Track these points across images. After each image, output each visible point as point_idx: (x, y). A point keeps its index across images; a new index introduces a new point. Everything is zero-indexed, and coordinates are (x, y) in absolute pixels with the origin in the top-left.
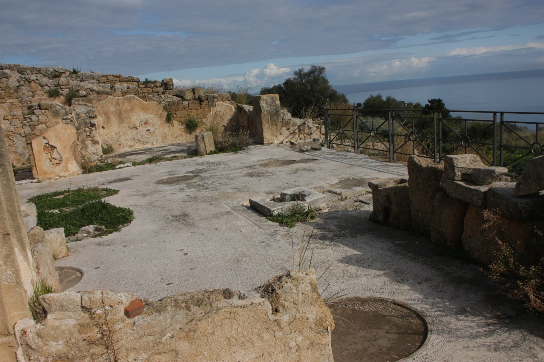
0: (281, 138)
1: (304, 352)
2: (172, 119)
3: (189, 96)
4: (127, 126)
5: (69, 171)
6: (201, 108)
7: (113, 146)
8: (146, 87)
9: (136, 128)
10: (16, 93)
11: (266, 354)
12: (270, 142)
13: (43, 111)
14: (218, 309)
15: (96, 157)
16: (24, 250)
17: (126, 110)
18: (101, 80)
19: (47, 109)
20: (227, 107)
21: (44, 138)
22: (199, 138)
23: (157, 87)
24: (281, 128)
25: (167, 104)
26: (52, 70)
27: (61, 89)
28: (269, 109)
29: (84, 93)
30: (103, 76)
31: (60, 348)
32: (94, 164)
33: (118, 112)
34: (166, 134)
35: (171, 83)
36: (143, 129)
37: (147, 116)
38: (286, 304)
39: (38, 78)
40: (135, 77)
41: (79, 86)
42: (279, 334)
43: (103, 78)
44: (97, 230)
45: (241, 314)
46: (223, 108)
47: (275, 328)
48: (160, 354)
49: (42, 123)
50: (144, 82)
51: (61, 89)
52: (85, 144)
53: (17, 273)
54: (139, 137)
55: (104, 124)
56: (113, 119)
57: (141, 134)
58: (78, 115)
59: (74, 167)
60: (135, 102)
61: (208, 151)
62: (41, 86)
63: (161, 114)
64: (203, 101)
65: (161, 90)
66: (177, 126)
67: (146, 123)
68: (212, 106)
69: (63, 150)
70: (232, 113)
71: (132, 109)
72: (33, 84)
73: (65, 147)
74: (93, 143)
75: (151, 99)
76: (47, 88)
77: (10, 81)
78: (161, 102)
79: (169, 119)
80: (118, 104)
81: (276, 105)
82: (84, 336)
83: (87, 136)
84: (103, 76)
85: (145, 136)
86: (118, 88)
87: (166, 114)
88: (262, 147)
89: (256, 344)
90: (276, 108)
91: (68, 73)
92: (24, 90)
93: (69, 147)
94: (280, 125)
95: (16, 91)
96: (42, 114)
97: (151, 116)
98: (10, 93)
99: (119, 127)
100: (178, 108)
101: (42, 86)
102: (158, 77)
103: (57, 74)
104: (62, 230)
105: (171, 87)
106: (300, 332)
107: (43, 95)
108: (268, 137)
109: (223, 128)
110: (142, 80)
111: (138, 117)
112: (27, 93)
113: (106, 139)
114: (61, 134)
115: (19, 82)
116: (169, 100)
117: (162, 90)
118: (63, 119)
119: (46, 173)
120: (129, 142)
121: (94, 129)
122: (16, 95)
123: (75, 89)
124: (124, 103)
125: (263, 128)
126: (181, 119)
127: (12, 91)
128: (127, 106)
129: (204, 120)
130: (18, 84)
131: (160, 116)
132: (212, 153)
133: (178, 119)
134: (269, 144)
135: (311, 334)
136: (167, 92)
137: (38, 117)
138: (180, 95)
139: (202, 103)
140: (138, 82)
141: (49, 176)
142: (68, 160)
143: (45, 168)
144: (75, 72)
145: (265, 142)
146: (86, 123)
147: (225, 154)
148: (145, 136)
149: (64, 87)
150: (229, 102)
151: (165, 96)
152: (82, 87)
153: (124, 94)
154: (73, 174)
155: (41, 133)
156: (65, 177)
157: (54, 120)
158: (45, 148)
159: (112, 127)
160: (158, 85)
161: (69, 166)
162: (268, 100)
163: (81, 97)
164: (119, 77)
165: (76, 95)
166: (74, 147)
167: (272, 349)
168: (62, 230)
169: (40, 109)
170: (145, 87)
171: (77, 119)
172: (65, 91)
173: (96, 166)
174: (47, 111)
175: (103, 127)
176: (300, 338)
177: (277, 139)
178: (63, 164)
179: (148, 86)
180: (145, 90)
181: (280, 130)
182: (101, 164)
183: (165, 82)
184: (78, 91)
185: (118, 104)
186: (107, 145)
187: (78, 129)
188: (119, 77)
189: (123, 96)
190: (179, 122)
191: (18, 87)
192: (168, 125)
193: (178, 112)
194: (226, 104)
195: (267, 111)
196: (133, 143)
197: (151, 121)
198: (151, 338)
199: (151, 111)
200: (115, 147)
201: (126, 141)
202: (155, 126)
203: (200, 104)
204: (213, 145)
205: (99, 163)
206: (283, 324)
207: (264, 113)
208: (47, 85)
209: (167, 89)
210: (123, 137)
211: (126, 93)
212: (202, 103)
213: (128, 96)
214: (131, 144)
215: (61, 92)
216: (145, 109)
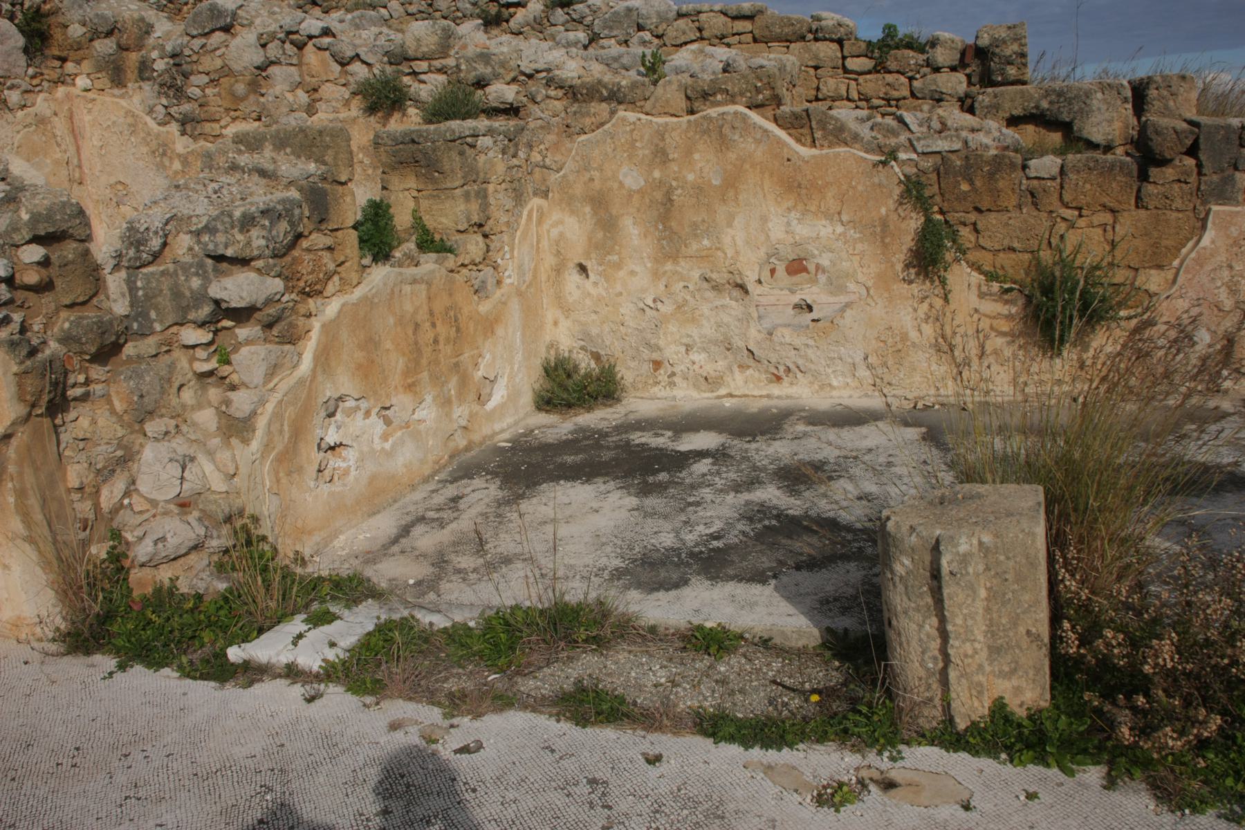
3: (1108, 122)
4: (696, 274)
6: (1139, 202)
8: (880, 68)
9: (742, 288)
10: (252, 98)
17: (700, 190)
23: (937, 70)
25: (927, 164)
27: (414, 74)
30: (680, 15)
33: (659, 195)
34: (904, 337)
36: (777, 296)
37: (803, 231)
43: (681, 23)
51: (414, 74)
54: (754, 335)
55: (587, 255)
56: (632, 230)
57: (767, 324)
60: (747, 145)
61: (970, 708)
62: (343, 65)
63: (884, 223)
64: (1163, 162)
65: (957, 83)
66: (974, 300)
67: (797, 267)
71: (731, 183)
75: (839, 135)
77: (236, 42)
78: (892, 155)
79: (927, 259)
80: (661, 155)
84: (680, 15)
85: (786, 335)
86: (678, 71)
87: (915, 222)
95: (255, 87)
97: (826, 229)
98: (233, 94)
99: (656, 275)
100: (996, 193)
105: (1012, 71)
107: (347, 103)
111: (758, 227)
112: (290, 97)
113: (594, 331)
115: (264, 46)
116: (942, 145)
124: (689, 152)
126: (1005, 259)
128: (705, 165)
129: (1153, 280)
130: (258, 57)
131: (882, 233)
133: (986, 259)
136: (985, 97)
139: (1153, 172)
140: (840, 42)
149: (423, 66)
152: (503, 64)
153: (699, 97)
159: (621, 274)
160: (942, 56)
164: (750, 18)
170: (874, 70)
175: (583, 269)
179: (892, 65)
180: (872, 85)
183: (984, 41)
185: (661, 155)
186: (597, 357)
188: (750, 18)
189: (692, 112)
190: (991, 277)
193: (992, 217)
196: (721, 365)
197: (825, 261)
199: (832, 203)
200: (626, 373)
203: (1143, 177)
209: (987, 80)
210: (672, 328)
211: (705, 96)
212: (1153, 172)
213: (713, 112)
214: (709, 369)
215: (414, 87)
216: (797, 188)
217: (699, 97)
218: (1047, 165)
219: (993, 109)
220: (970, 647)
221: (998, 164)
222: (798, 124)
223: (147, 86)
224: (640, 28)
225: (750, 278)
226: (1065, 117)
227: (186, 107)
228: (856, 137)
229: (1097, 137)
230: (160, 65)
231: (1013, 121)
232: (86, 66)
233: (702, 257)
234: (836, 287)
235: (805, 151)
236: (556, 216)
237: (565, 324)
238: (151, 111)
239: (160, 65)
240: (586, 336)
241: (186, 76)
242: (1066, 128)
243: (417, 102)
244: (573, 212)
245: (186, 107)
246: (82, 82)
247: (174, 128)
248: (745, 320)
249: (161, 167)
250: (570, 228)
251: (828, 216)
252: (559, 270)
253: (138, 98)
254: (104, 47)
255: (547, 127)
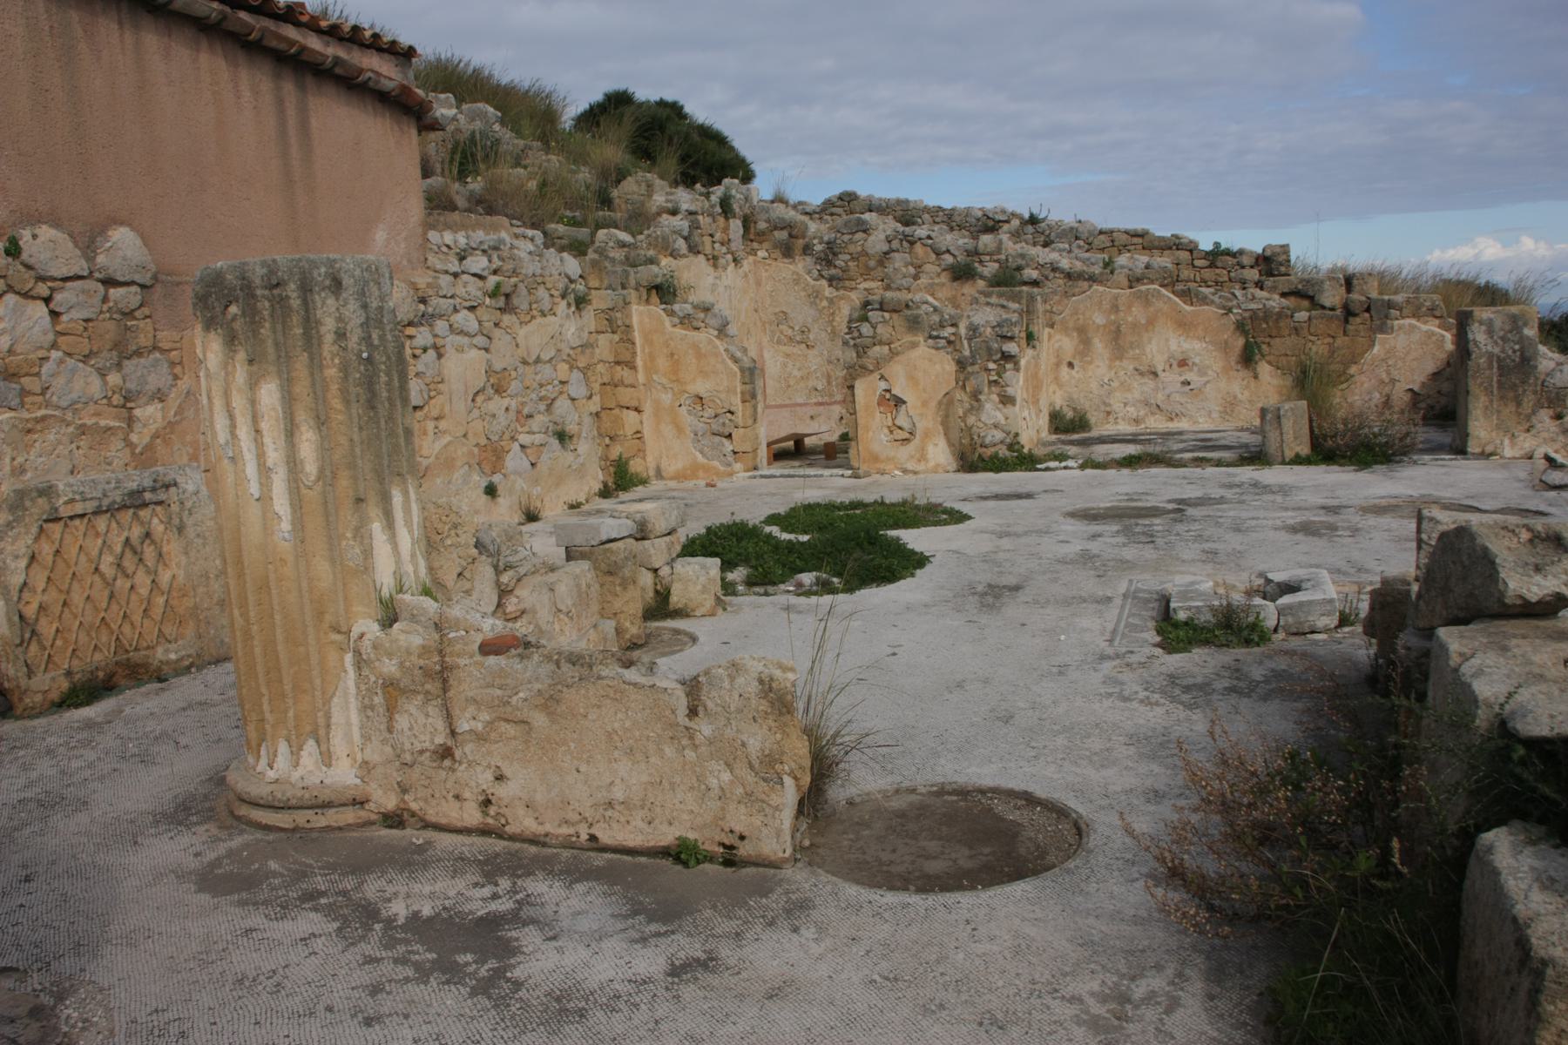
0: (1527, 443)
1: (732, 806)
2: (1257, 357)
3: (1332, 296)
5: (926, 460)
7: (1089, 416)
8: (1212, 265)
9: (1155, 374)
11: (666, 784)
12: (1489, 449)
13: (887, 315)
14: (599, 678)
15: (999, 435)
16: (390, 525)
17: (1135, 326)
18: (1096, 242)
19: (895, 311)
20: (1430, 334)
21: (882, 377)
22: (1269, 416)
23: (1243, 267)
24: (1534, 413)
25: (1247, 315)
26: (980, 214)
27: (981, 262)
28: (1496, 350)
29: (1034, 274)
31: (393, 669)
32: (989, 452)
35: (1282, 258)
36: (1172, 378)
37: (1186, 346)
38: (710, 704)
39: (933, 235)
40: (1189, 234)
41: (1023, 256)
42: (690, 755)
43: (1102, 237)
44: (818, 581)
45: (633, 697)
46: (1416, 337)
47: (685, 742)
48: (507, 721)
49: (881, 343)
50: (1207, 253)
51: (981, 262)
52: (978, 400)
53: (368, 553)
54: (1160, 397)
56: (1098, 345)
57: (1167, 391)
58: (974, 330)
59: (940, 453)
60: (1160, 304)
61: (1289, 454)
64: (1355, 315)
65: (1253, 275)
67: (1183, 363)
68: (1382, 329)
69: (920, 412)
70: (1444, 356)
71: (1151, 322)
72: (918, 248)
73: (925, 404)
74: (1002, 402)
75: (1204, 300)
76: (949, 259)
77: (872, 238)
78: (1230, 310)
79: (1248, 358)
80: (1115, 308)
81: (1522, 340)
82: (422, 662)
83: (990, 382)
84: (1101, 232)
85: (1177, 397)
86: (1122, 267)
87: (1241, 342)
88: (1461, 462)
89: (652, 760)
90: (1522, 350)
91: (1016, 223)
92: (898, 260)
93: (933, 404)
94: (1528, 402)
95: (881, 263)
96: (885, 322)
97: (1197, 345)
98: (867, 267)
99: (1110, 368)
100: (1279, 328)
101: (938, 254)
102: (1253, 241)
103: (991, 223)
104: (718, 561)
105: (1283, 269)
106: (727, 765)
107: (939, 275)
108: (1483, 434)
109: (1407, 397)
110: (1206, 245)
111: (1164, 344)
114: (922, 372)
116: (1253, 306)
117: (1257, 277)
118: (931, 337)
119: (875, 458)
120: (1131, 409)
121: (1009, 366)
122: (879, 272)
123: (1012, 264)
124: (1130, 307)
125: (1471, 406)
126: (1284, 360)
127: (872, 263)
128: (1138, 313)
130: (885, 248)
131: (1225, 347)
132: (1298, 460)
134: (1484, 455)
135: (750, 778)
136: (1269, 282)
137: (874, 328)
138: (1306, 293)
140: (1191, 251)
141: (882, 466)
142: (927, 435)
143: (875, 447)
144: (1033, 220)
145: (1473, 447)
146: (989, 349)
147: (1335, 468)
148: (1177, 397)
150: (1437, 322)
151: (1245, 295)
153: (1134, 281)
154: (935, 470)
155: (878, 366)
156: (915, 473)
157: (909, 338)
158: (882, 401)
161: (930, 449)
162: (1498, 323)
163: (1025, 283)
165: (1013, 277)
166: (947, 403)
167: (677, 779)
168: (718, 561)
169: (881, 309)
171: (970, 340)
172: (990, 268)
173: (995, 456)
174: (895, 316)
175: (1071, 365)
176: (726, 776)
177: (1513, 445)
178: (916, 441)
181: (1528, 418)
182: (1008, 453)
183: (1268, 253)
184: (1019, 269)
185: (1115, 308)
186: (1074, 409)
187: (961, 364)
191: (886, 253)
192: (1244, 373)
194: (1424, 327)
195: (1490, 356)
198: (499, 692)
200: (1093, 418)
201: (1126, 404)
202: (1205, 374)
203: (1346, 321)
204: (1306, 438)
205: (1003, 452)
206: (699, 738)
207: (1479, 360)
208: (948, 251)
211: (1138, 280)
213: (1143, 288)
215: (980, 269)
216: (1184, 325)
217: (1134, 281)
218: (1302, 316)
219: (1273, 289)
220: (1289, 436)
221: (1280, 315)
222: (1186, 295)
223: (808, 259)
224: (1077, 238)
225: (1159, 369)
226: (1311, 293)
227: (833, 271)
228: (1213, 302)
229: (1327, 304)
230: (818, 248)
231: (1284, 295)
232: (766, 245)
233: (1135, 358)
234: (1202, 373)
235: (1188, 308)
236: (1058, 337)
237: (1059, 393)
238: (809, 272)
239: (818, 248)
240: (1071, 399)
241: (835, 254)
242: (1311, 298)
243: (982, 277)
244: (1068, 335)
245: (833, 271)
246: (762, 254)
247: (824, 283)
248: (1156, 390)
249: (813, 304)
250: (1067, 344)
251: (1198, 338)
252: (1058, 365)
253: (802, 265)
254: (782, 235)
255: (1054, 293)
